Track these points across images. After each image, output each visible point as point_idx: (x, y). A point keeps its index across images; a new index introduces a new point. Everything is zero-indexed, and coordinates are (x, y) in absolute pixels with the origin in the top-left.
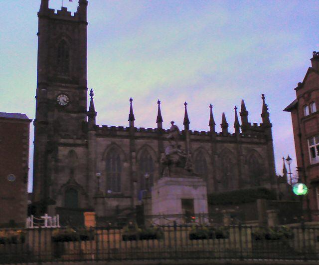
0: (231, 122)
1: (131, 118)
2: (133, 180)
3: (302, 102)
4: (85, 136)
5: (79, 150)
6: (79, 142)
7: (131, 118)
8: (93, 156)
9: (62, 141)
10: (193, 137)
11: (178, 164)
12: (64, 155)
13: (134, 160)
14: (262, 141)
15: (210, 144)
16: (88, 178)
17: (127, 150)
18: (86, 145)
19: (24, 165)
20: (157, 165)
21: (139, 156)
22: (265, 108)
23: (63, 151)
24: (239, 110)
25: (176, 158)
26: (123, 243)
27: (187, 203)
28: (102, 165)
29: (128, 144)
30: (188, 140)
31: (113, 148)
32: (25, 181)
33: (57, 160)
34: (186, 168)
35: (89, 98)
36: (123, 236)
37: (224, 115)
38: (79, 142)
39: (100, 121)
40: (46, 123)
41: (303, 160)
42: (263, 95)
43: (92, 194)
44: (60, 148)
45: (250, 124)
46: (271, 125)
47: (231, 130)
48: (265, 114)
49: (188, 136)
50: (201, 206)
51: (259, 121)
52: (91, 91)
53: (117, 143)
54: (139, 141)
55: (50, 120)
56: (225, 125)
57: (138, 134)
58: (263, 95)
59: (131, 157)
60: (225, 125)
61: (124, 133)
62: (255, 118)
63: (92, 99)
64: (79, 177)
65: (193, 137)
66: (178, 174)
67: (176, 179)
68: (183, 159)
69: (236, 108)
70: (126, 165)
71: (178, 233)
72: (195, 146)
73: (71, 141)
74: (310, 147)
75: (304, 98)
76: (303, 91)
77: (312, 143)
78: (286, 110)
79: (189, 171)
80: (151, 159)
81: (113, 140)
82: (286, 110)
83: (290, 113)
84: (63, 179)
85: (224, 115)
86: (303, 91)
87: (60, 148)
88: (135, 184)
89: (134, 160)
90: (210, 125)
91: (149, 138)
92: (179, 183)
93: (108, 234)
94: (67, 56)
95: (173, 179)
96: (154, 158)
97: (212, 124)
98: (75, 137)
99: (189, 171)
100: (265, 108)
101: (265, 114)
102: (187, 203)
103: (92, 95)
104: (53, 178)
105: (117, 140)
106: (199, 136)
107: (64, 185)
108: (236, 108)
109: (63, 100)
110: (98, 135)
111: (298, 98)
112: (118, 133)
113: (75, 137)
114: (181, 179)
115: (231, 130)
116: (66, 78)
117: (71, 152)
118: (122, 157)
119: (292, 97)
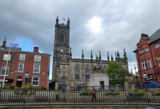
0: (114, 57)
1: (83, 56)
2: (83, 76)
3: (139, 49)
4: (68, 61)
5: (66, 66)
6: (66, 63)
7: (83, 56)
8: (71, 68)
9: (61, 63)
10: (102, 62)
11: (98, 69)
12: (61, 68)
13: (84, 69)
14: (124, 63)
15: (108, 64)
16: (69, 75)
17: (81, 66)
18: (69, 65)
19: (48, 70)
20: (91, 71)
21: (85, 68)
22: (125, 53)
23: (61, 66)
24: (117, 54)
25: (98, 67)
26: (80, 96)
27: (102, 83)
28: (74, 71)
29: (82, 64)
30: (101, 63)
31: (77, 65)
32: (48, 74)
33: (59, 69)
34: (101, 70)
35: (70, 50)
36: (13, 79)
37: (112, 55)
38: (66, 63)
39: (73, 57)
40: (56, 58)
41: (52, 105)
42: (124, 49)
43: (70, 80)
44: (60, 65)
45: (120, 58)
46: (127, 59)
47: (114, 60)
48: (125, 55)
49: (101, 62)
50: (107, 83)
51: (123, 57)
52: (71, 48)
53: (78, 64)
54: (84, 63)
55: (58, 57)
56: (112, 59)
57: (85, 61)
58: (124, 49)
59: (83, 68)
60: (112, 59)
61: (81, 61)
62: (122, 56)
63: (71, 50)
64: (66, 75)
65: (102, 62)
66: (98, 72)
67: (98, 74)
68: (100, 67)
69: (116, 53)
70: (81, 71)
71: (100, 93)
72: (103, 65)
73: (64, 63)
74: (142, 64)
75: (140, 48)
76: (139, 46)
77: (143, 62)
78: (133, 52)
79: (102, 72)
80: (89, 69)
81: (77, 63)
82: (133, 52)
83: (135, 53)
84: (61, 75)
85: (112, 55)
86: (139, 46)
87: (60, 65)
88: (84, 77)
89: (84, 69)
90: (108, 58)
91: (88, 62)
92: (99, 76)
93: (74, 93)
94: (63, 38)
95: (97, 74)
96: (90, 69)
97: (108, 58)
98: (65, 62)
99: (102, 72)
100: (125, 53)
101: (125, 55)
102: (102, 83)
103: (70, 49)
104: (58, 75)
105: (78, 63)
106: (104, 62)
107: (62, 77)
108: (116, 53)
109: (62, 51)
110: (72, 61)
111: (138, 48)
112: (79, 61)
113: (65, 62)
114: (100, 74)
115: (114, 60)
116: (63, 44)
117: (64, 66)
118: (80, 68)
119: (136, 48)
